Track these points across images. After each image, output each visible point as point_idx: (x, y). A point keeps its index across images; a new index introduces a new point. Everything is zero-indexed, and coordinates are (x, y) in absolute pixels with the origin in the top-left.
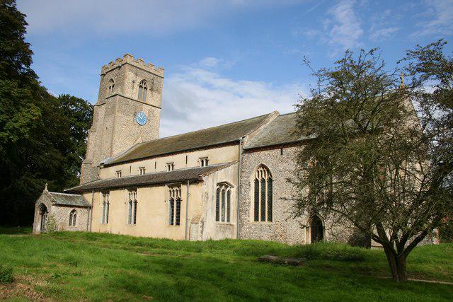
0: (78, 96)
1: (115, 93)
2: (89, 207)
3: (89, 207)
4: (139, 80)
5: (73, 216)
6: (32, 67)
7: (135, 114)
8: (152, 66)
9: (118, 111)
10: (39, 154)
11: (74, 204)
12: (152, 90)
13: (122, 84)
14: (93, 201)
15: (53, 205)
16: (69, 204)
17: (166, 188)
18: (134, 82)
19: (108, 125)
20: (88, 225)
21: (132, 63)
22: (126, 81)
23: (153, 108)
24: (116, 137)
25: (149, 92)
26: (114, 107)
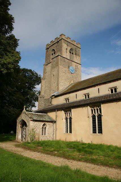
0: (29, 68)
1: (57, 55)
2: (53, 122)
3: (53, 122)
4: (69, 49)
5: (44, 128)
6: (14, 32)
7: (69, 67)
8: (75, 41)
9: (60, 65)
10: (13, 96)
11: (44, 120)
12: (76, 54)
13: (60, 50)
14: (56, 117)
15: (31, 120)
16: (41, 119)
17: (89, 108)
18: (67, 49)
19: (55, 73)
20: (53, 134)
21: (65, 39)
22: (63, 48)
23: (77, 64)
24: (60, 79)
25: (74, 55)
26: (57, 63)
